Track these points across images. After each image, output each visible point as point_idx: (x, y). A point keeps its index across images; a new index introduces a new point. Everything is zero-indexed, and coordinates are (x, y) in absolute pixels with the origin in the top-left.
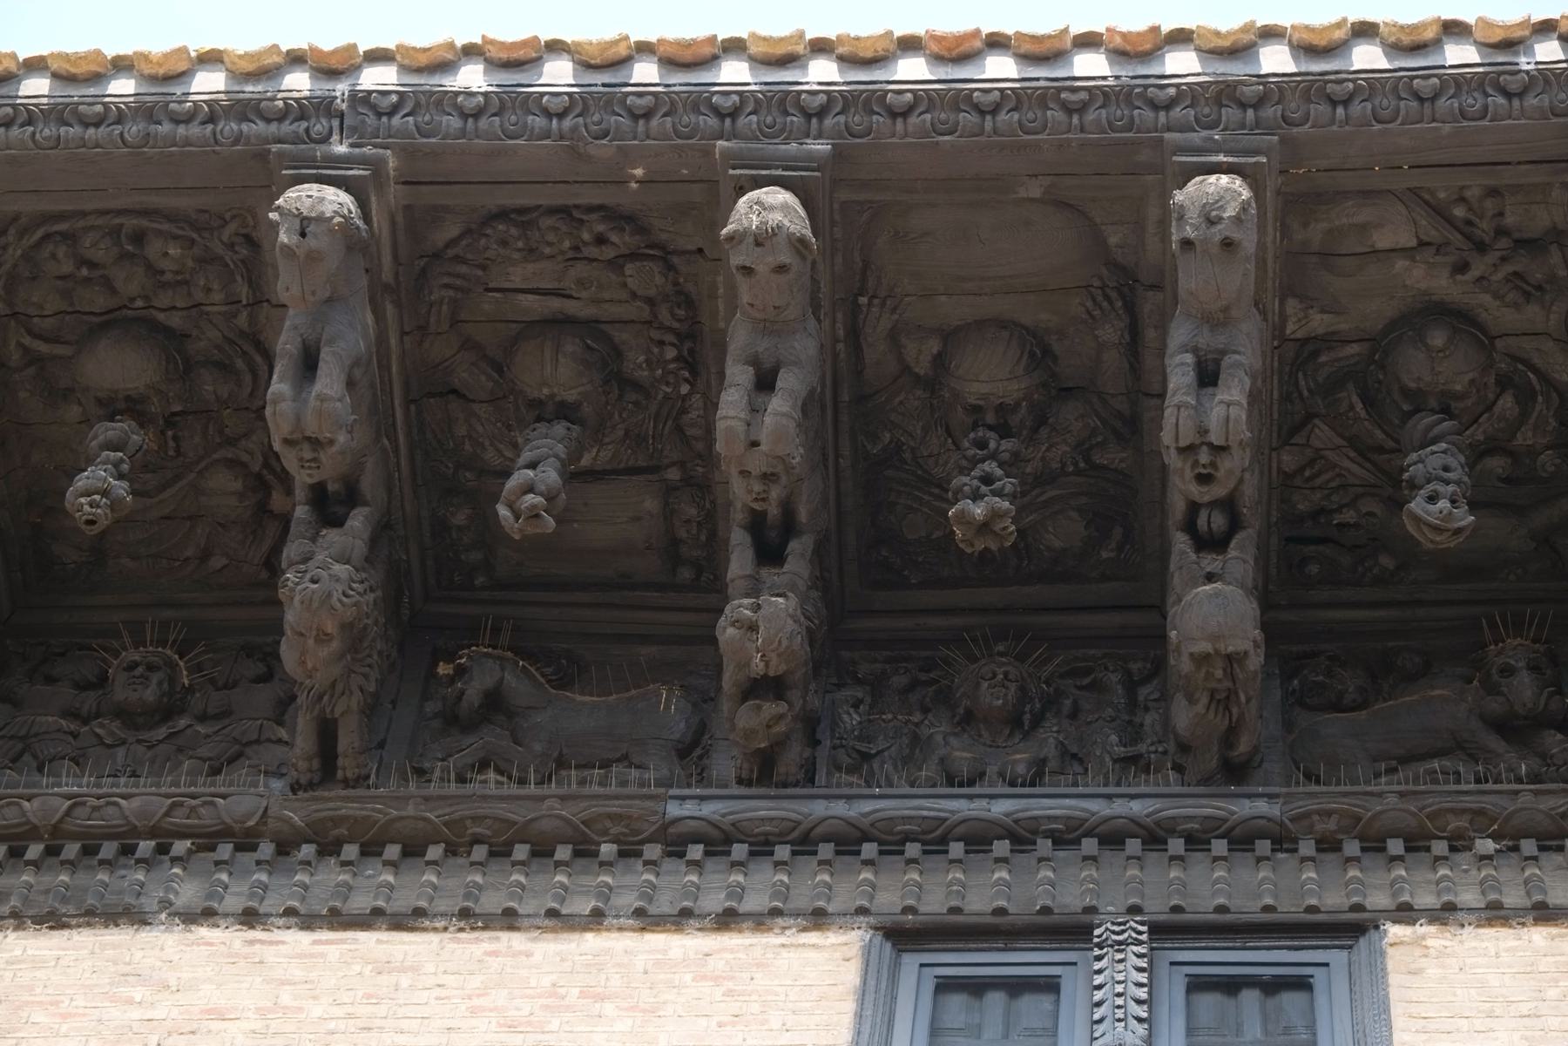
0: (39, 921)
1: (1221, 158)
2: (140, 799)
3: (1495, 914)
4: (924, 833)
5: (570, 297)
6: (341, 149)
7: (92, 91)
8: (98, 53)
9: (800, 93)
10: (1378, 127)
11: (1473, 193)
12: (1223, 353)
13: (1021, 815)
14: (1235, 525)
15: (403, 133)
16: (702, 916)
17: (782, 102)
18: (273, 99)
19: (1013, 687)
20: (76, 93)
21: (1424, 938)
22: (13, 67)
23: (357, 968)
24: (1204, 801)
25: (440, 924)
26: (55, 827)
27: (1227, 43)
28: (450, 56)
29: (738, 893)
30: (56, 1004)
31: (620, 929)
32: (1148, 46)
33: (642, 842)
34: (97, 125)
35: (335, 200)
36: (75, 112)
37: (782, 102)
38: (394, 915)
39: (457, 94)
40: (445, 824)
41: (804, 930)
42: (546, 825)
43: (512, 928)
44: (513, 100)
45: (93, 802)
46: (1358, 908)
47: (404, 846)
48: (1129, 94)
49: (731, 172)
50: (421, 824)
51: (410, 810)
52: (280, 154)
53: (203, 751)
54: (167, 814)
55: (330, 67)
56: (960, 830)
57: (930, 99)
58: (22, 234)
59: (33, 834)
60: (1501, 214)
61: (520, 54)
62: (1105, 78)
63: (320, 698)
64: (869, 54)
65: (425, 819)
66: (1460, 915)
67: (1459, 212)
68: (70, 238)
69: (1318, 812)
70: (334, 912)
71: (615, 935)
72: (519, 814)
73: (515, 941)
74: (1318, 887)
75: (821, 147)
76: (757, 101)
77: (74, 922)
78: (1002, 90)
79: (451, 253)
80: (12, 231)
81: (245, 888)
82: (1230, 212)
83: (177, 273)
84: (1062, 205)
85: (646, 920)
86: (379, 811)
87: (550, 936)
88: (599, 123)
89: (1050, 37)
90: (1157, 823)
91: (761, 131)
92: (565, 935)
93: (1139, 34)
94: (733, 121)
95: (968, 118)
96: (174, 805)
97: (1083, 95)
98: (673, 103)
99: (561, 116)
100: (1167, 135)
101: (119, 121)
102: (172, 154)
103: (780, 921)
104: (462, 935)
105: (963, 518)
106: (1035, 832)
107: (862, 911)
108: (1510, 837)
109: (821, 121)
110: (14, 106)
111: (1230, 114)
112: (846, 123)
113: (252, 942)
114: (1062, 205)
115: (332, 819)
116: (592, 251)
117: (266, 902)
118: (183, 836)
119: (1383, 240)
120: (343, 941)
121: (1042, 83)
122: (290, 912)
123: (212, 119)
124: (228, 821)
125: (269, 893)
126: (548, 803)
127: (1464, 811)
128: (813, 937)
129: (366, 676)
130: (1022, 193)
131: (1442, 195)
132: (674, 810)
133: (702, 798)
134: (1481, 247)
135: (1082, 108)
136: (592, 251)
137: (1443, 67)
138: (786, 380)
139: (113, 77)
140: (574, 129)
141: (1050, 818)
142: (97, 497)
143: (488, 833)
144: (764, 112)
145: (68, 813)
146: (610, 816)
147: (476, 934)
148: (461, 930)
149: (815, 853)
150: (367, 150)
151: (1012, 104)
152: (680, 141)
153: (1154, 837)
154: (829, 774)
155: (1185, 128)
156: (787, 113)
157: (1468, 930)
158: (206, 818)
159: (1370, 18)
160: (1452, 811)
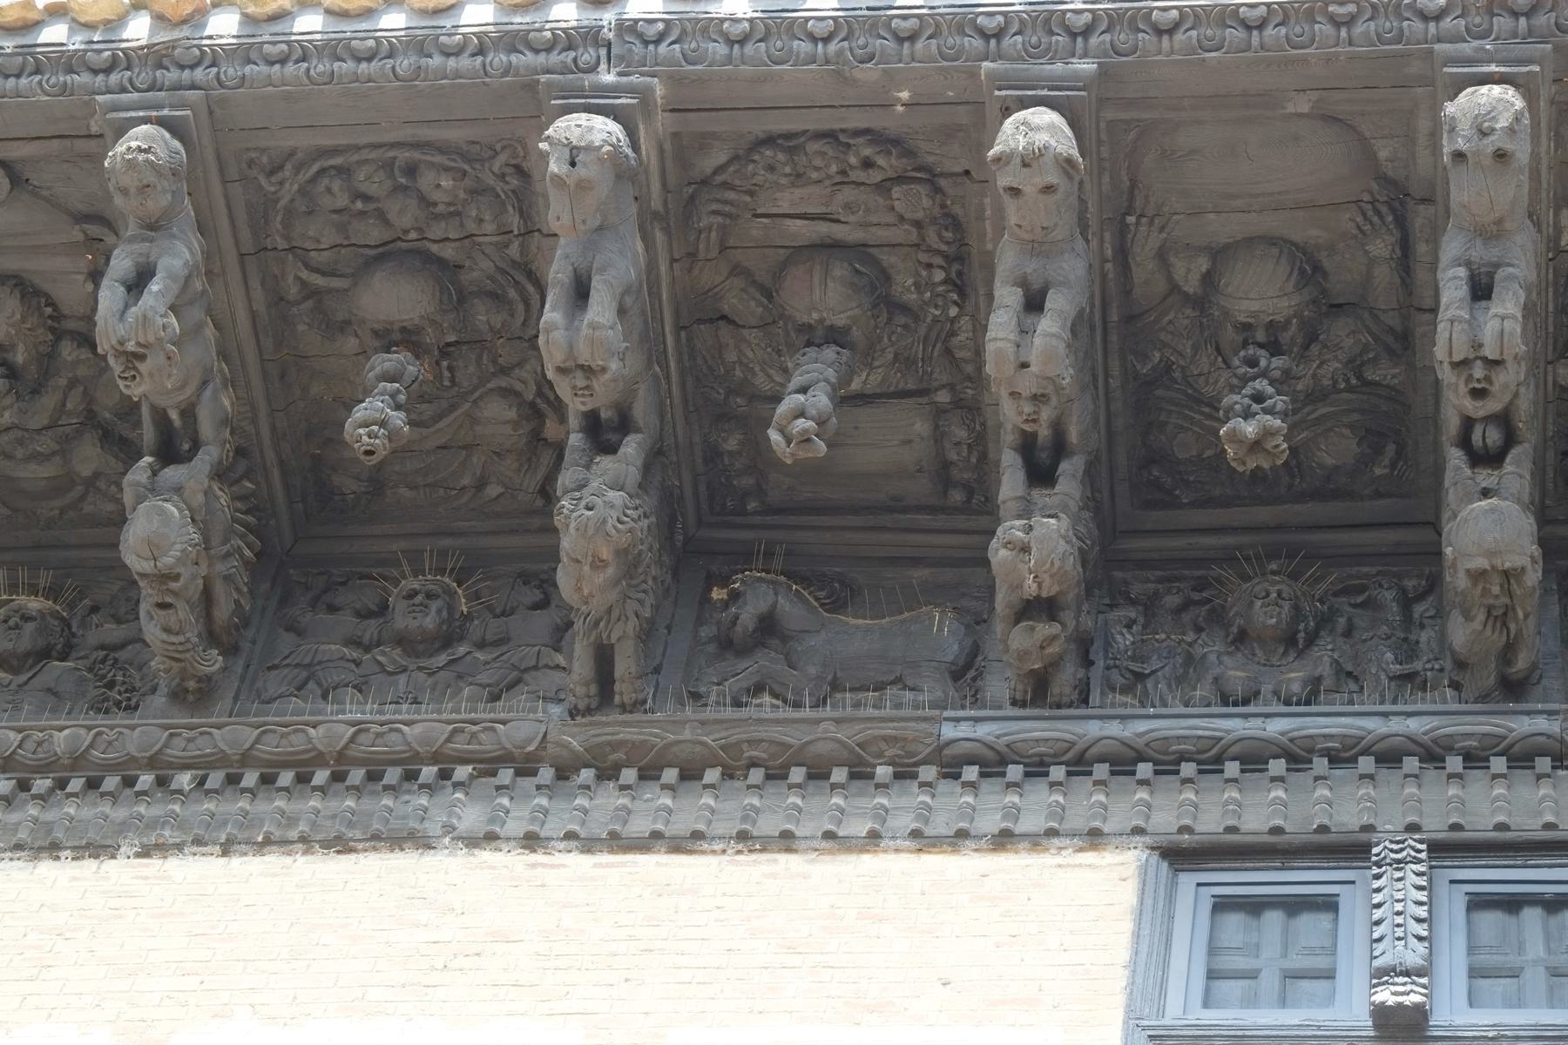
0: (327, 845)
1: (1493, 68)
4: (1199, 752)
5: (838, 221)
6: (608, 78)
7: (364, 26)
13: (1296, 734)
14: (1510, 440)
15: (671, 61)
17: (1047, 21)
18: (540, 30)
19: (1287, 605)
25: (718, 847)
31: (897, 850)
33: (917, 764)
34: (369, 60)
35: (603, 130)
36: (348, 48)
37: (1047, 21)
38: (672, 838)
39: (722, 21)
40: (722, 748)
41: (1081, 850)
42: (822, 748)
43: (789, 850)
44: (779, 26)
45: (376, 728)
49: (997, 93)
50: (698, 748)
51: (687, 734)
53: (483, 678)
56: (1235, 749)
59: (319, 760)
63: (597, 623)
68: (344, 172)
70: (614, 835)
72: (793, 737)
75: (1086, 66)
76: (1022, 21)
77: (360, 846)
79: (719, 179)
80: (288, 166)
86: (656, 736)
87: (828, 858)
90: (1435, 741)
91: (1026, 51)
94: (998, 42)
95: (1235, 34)
98: (937, 25)
99: (826, 40)
100: (1437, 47)
102: (442, 87)
103: (1056, 841)
104: (740, 858)
105: (1234, 437)
106: (1311, 751)
107: (1138, 831)
109: (1086, 40)
113: (534, 866)
115: (609, 743)
120: (623, 864)
122: (570, 836)
123: (481, 51)
124: (509, 746)
126: (823, 725)
130: (1291, 109)
132: (949, 731)
133: (977, 720)
138: (1054, 301)
140: (840, 53)
143: (764, 756)
144: (1029, 31)
145: (352, 740)
146: (885, 739)
147: (754, 857)
148: (739, 852)
151: (1279, 19)
152: (945, 63)
155: (1456, 39)
156: (1051, 33)
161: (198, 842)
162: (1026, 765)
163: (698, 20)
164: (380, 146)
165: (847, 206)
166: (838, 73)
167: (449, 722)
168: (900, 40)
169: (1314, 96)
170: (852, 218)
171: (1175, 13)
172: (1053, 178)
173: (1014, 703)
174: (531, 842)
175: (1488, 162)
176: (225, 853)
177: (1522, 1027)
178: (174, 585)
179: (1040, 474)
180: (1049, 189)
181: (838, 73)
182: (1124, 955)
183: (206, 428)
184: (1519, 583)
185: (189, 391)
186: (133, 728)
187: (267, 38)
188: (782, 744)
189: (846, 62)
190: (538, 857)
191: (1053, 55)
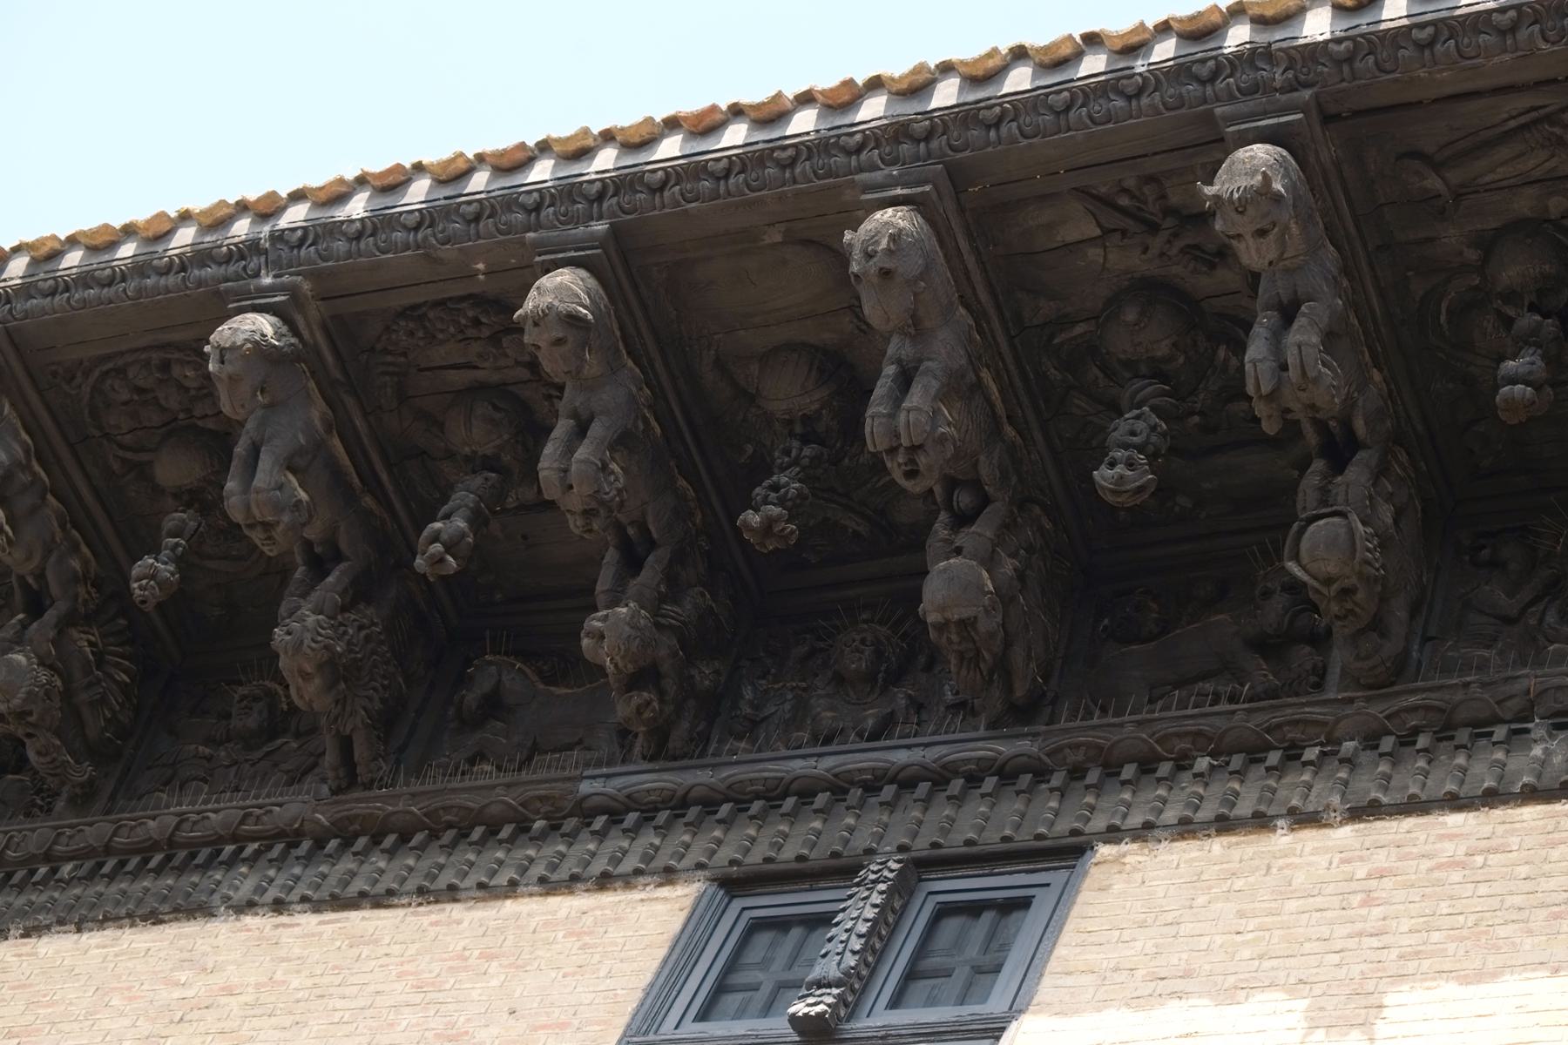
0: (144, 919)
1: (899, 191)
2: (220, 813)
3: (1186, 829)
4: (768, 790)
5: (476, 368)
6: (267, 280)
7: (107, 257)
8: (106, 226)
9: (581, 183)
10: (1025, 142)
11: (1130, 183)
12: (920, 361)
13: (837, 770)
14: (985, 501)
15: (310, 262)
16: (586, 880)
17: (570, 193)
18: (221, 246)
19: (868, 651)
20: (910, 108)
21: (1124, 856)
22: (57, 246)
23: (338, 944)
24: (980, 744)
25: (405, 901)
26: (170, 839)
27: (904, 86)
28: (344, 189)
29: (1231, 800)
30: (129, 989)
31: (531, 895)
32: (846, 98)
33: (564, 818)
34: (109, 285)
35: (263, 325)
36: (93, 277)
37: (570, 193)
38: (374, 896)
39: (342, 222)
40: (425, 815)
41: (661, 885)
42: (495, 809)
43: (456, 900)
45: (194, 817)
46: (1075, 833)
47: (1140, 764)
48: (827, 144)
49: (538, 259)
50: (408, 817)
51: (401, 807)
52: (227, 291)
53: (285, 767)
54: (242, 822)
55: (267, 209)
56: (794, 786)
57: (677, 173)
58: (86, 374)
59: (155, 846)
60: (1164, 197)
61: (390, 180)
62: (808, 133)
63: (336, 719)
64: (637, 140)
65: (411, 812)
66: (1157, 832)
67: (1124, 201)
68: (121, 372)
69: (1070, 746)
70: (334, 897)
71: (527, 900)
72: (473, 802)
73: (455, 911)
74: (1049, 815)
75: (600, 227)
76: (552, 195)
77: (166, 918)
78: (729, 157)
79: (379, 347)
80: (79, 374)
81: (1255, 795)
82: (884, 243)
83: (199, 389)
84: (807, 242)
85: (549, 887)
86: (379, 808)
87: (480, 905)
88: (443, 231)
89: (764, 104)
90: (944, 767)
92: (492, 903)
93: (831, 90)
96: (246, 816)
97: (790, 152)
98: (493, 206)
99: (417, 228)
100: (856, 177)
101: (124, 280)
102: (159, 302)
103: (641, 879)
104: (421, 909)
106: (852, 783)
107: (700, 866)
108: (1220, 749)
109: (998, 129)
110: (55, 278)
111: (905, 148)
112: (618, 203)
113: (277, 926)
114: (807, 242)
115: (348, 818)
116: (471, 332)
117: (918, 840)
118: (254, 840)
119: (1071, 234)
120: (337, 921)
121: (760, 146)
122: (304, 899)
123: (183, 268)
125: (1204, 803)
126: (498, 790)
127: (1187, 734)
128: (665, 892)
129: (370, 699)
130: (768, 241)
131: (1103, 190)
132: (585, 787)
133: (608, 776)
134: (1153, 228)
135: (793, 162)
136: (471, 332)
137: (1072, 80)
138: (596, 430)
139: (124, 242)
140: (425, 238)
141: (969, 760)
142: (144, 582)
145: (177, 827)
146: (540, 798)
147: (431, 907)
148: (420, 904)
149: (1452, 738)
150: (285, 279)
153: (939, 778)
154: (720, 741)
155: (874, 168)
156: (575, 202)
157: (1165, 844)
158: (267, 824)
159: (1096, 28)
160: (1178, 735)
161: (61, 922)
162: (642, 811)
163: (326, 224)
164: (137, 350)
165: (480, 356)
166: (427, 256)
167: (242, 808)
168: (469, 222)
169: (782, 227)
170: (486, 365)
171: (535, 195)
172: (558, 333)
173: (644, 758)
174: (279, 906)
175: (875, 280)
176: (79, 930)
177: (904, 1027)
178: (32, 719)
179: (632, 563)
180: (559, 342)
181: (427, 256)
182: (648, 977)
183: (55, 589)
184: (975, 630)
185: (36, 561)
186: (33, 830)
187: (42, 276)
188: (467, 808)
189: (432, 246)
190: (284, 919)
191: (576, 220)
